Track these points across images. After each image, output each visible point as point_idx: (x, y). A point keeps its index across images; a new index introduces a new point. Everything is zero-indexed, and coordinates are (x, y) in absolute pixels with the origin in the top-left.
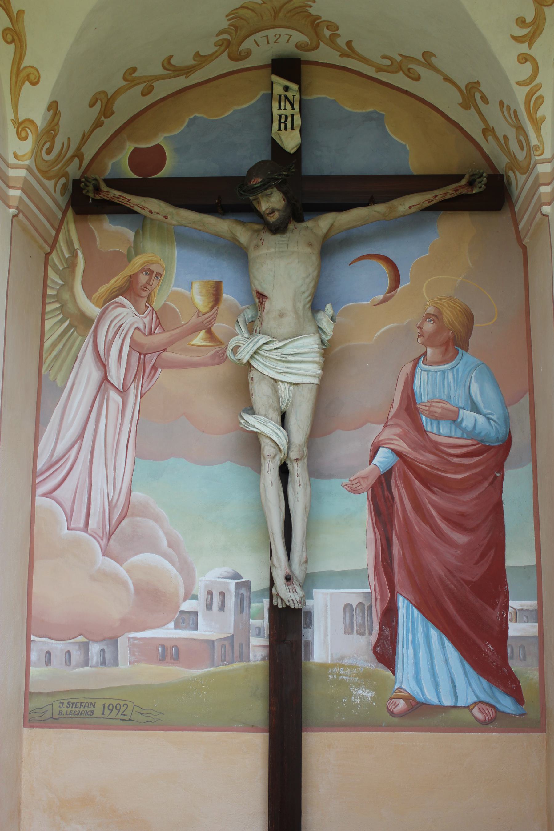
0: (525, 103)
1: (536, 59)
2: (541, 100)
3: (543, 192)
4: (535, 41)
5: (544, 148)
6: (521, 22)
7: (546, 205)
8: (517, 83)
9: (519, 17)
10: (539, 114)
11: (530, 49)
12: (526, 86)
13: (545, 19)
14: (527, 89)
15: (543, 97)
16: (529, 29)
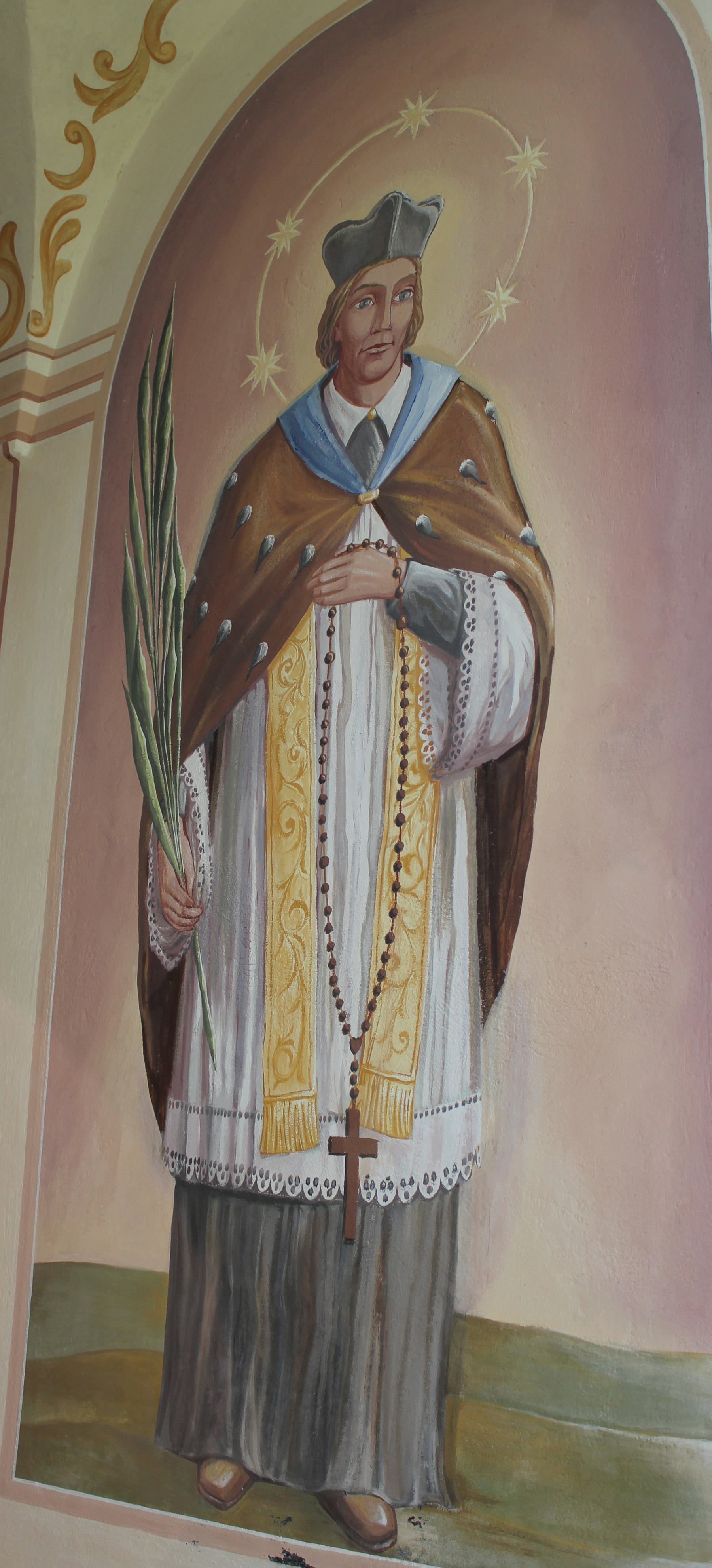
0: (46, 221)
1: (96, 146)
2: (74, 230)
3: (25, 410)
4: (108, 112)
5: (50, 324)
6: (103, 61)
7: (23, 439)
8: (47, 174)
9: (105, 49)
10: (63, 254)
11: (94, 122)
12: (61, 188)
13: (142, 82)
14: (60, 194)
15: (80, 227)
16: (108, 84)
